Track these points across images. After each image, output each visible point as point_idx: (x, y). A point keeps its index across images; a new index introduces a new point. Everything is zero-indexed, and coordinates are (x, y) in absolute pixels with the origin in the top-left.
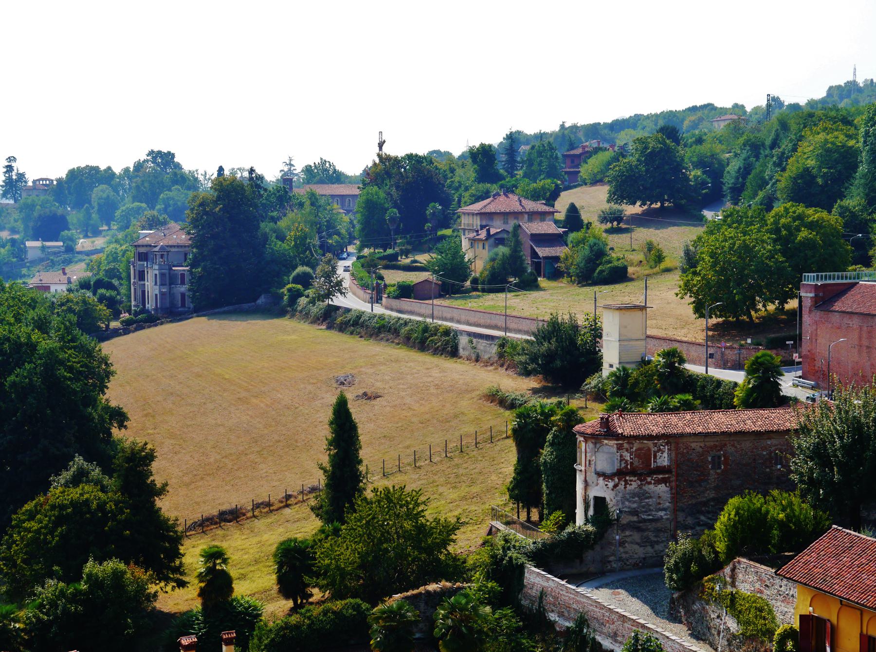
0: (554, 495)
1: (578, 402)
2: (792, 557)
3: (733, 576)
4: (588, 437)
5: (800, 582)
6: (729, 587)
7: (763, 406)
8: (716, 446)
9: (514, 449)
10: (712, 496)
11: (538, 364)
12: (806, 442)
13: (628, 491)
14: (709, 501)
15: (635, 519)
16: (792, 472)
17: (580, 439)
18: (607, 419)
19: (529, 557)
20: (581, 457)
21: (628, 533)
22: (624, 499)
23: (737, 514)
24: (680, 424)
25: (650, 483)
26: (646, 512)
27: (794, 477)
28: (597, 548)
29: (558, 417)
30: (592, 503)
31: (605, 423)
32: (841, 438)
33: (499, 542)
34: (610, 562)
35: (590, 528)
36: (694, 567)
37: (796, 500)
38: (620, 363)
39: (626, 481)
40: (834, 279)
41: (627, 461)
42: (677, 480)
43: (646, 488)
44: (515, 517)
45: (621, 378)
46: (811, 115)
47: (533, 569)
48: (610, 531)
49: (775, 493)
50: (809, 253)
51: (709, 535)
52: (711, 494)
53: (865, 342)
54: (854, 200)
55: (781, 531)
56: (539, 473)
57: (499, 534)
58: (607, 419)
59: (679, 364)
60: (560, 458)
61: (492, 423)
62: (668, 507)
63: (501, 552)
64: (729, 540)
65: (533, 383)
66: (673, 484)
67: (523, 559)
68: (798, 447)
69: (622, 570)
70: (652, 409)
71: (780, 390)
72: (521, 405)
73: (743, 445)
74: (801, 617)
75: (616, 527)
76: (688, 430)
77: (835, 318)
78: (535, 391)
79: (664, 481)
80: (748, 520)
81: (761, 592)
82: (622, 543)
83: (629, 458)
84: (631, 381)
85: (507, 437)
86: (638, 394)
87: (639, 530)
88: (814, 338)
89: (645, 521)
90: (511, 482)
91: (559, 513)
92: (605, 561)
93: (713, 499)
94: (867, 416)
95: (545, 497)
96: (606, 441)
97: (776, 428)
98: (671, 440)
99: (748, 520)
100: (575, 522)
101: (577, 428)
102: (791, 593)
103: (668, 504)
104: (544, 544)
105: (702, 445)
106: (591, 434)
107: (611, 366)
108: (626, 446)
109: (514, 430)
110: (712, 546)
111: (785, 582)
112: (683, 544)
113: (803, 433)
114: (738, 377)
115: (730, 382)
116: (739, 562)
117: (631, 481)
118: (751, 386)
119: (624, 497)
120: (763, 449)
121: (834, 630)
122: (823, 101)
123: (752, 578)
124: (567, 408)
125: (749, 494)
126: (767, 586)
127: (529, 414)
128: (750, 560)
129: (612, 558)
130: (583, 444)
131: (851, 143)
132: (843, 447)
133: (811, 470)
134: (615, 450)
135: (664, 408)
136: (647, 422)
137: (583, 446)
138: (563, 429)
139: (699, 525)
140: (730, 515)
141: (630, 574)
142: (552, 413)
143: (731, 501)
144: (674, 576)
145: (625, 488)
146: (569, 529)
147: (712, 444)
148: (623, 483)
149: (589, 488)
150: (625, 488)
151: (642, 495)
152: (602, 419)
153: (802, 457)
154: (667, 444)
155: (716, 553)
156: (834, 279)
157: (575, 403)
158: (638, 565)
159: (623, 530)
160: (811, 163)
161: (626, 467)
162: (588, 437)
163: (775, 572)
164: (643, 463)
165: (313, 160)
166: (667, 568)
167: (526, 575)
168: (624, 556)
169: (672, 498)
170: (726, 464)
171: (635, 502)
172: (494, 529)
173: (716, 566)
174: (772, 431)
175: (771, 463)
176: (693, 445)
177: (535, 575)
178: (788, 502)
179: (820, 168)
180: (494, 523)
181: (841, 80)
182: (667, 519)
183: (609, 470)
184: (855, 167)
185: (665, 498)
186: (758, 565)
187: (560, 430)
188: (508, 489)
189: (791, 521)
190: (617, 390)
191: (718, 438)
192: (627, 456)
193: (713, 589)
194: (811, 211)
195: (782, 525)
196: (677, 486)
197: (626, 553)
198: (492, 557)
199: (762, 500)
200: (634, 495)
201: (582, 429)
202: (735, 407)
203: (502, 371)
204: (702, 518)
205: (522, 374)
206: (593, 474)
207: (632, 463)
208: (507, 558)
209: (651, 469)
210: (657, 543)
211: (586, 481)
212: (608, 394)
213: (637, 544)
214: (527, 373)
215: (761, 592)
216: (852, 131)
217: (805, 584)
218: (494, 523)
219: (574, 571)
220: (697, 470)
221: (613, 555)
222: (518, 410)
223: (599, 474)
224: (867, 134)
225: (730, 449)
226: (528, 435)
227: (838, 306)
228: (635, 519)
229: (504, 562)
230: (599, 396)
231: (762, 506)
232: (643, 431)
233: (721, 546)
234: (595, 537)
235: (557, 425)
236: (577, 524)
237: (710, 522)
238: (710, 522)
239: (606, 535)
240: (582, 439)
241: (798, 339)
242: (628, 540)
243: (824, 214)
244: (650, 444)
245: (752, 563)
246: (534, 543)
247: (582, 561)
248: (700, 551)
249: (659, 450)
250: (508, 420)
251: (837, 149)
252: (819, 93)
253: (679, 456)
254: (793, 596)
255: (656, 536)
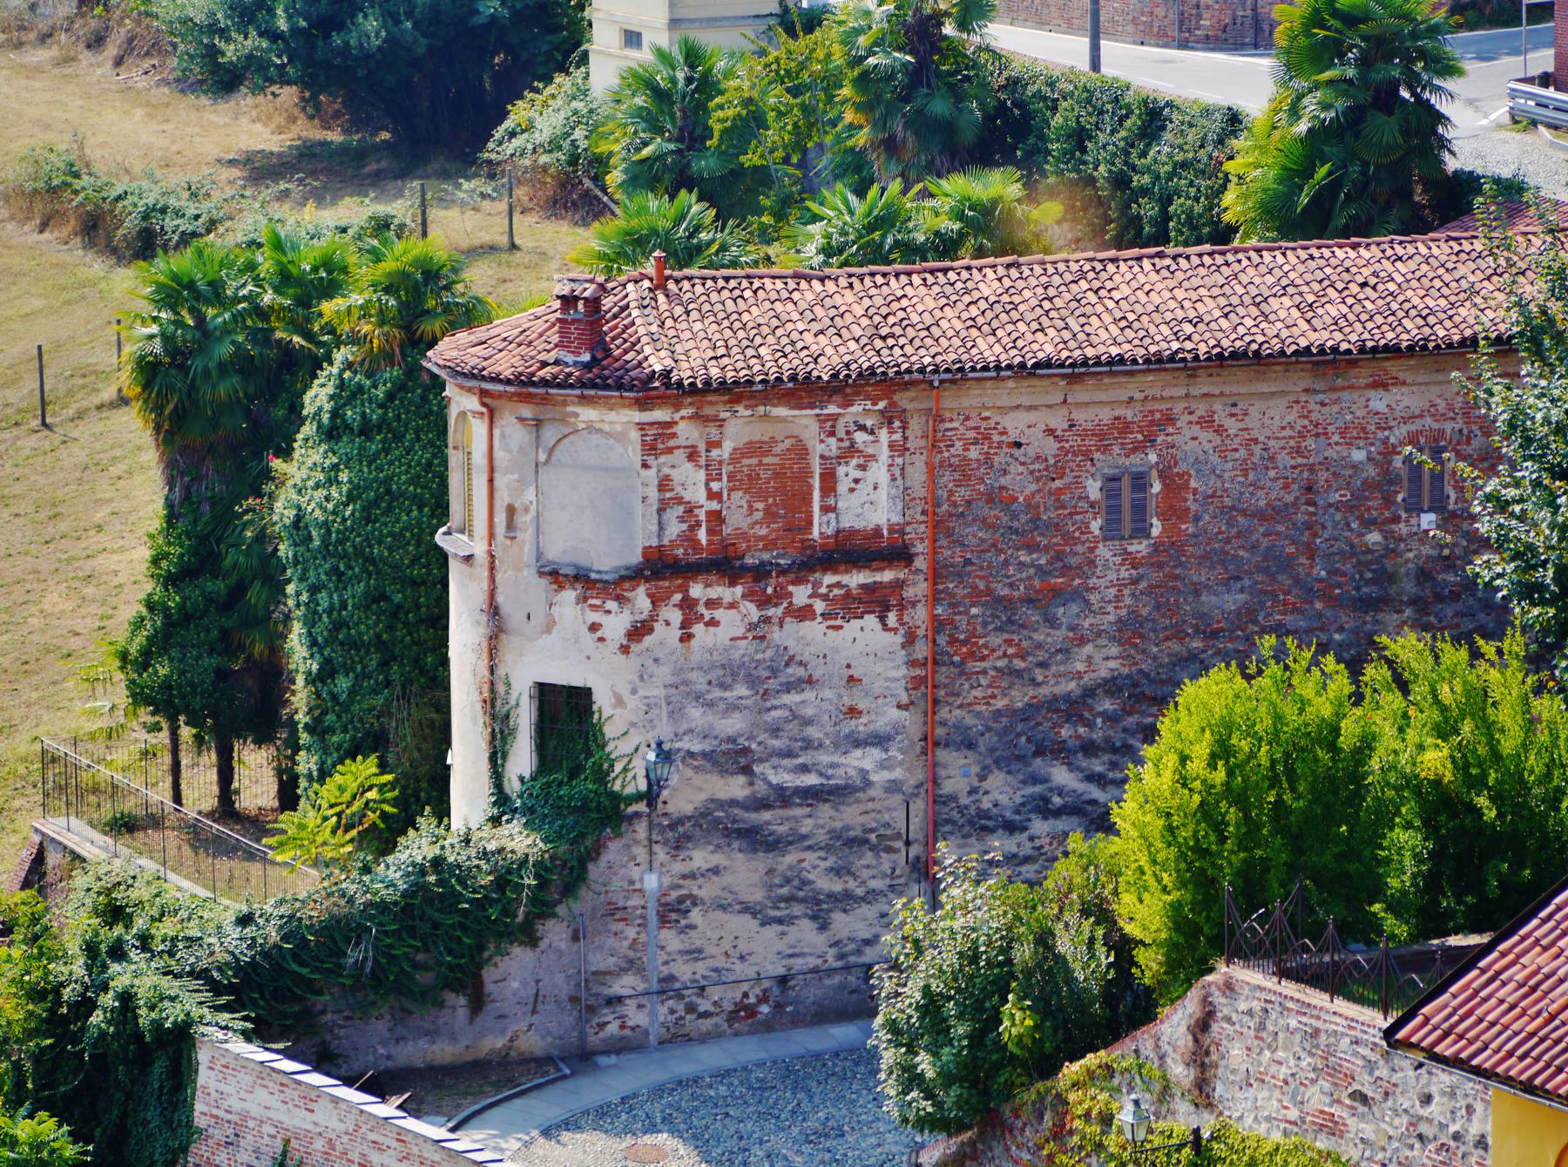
0: (343, 683)
1: (470, 220)
2: (1467, 960)
3: (1202, 1058)
4: (498, 392)
5: (1507, 1080)
6: (1183, 1107)
7: (1359, 230)
8: (1123, 426)
9: (149, 459)
10: (1104, 670)
11: (274, 36)
13: (696, 657)
14: (1089, 693)
15: (736, 787)
16: (1484, 544)
17: (461, 402)
18: (594, 304)
19: (216, 988)
20: (467, 488)
21: (701, 858)
22: (682, 693)
23: (1222, 752)
24: (951, 321)
25: (805, 613)
26: (790, 754)
27: (1492, 569)
28: (554, 933)
29: (357, 299)
30: (525, 720)
31: (585, 318)
33: (74, 920)
34: (615, 1001)
35: (519, 839)
36: (1016, 1021)
37: (1506, 683)
38: (674, 23)
39: (688, 604)
41: (690, 510)
42: (935, 598)
43: (791, 635)
44: (161, 795)
45: (680, 102)
47: (240, 1047)
48: (613, 851)
49: (1407, 647)
51: (1089, 863)
52: (1103, 660)
55: (1430, 827)
56: (271, 575)
57: (80, 881)
58: (594, 304)
59: (963, 25)
60: (374, 501)
61: (45, 332)
62: (898, 728)
63: (78, 968)
64: (1182, 884)
65: (263, 123)
66: (920, 615)
67: (188, 1002)
68: (1512, 425)
69: (675, 1038)
70: (828, 251)
71: (1443, 144)
72: (187, 238)
73: (1253, 421)
75: (641, 829)
76: (988, 350)
78: (261, 170)
79: (877, 601)
80: (1274, 781)
81: (1332, 1127)
82: (673, 911)
83: (700, 496)
84: (722, 114)
85: (123, 401)
86: (762, 177)
87: (755, 840)
89: (784, 797)
90: (138, 623)
91: (365, 768)
92: (589, 999)
93: (1111, 686)
95: (300, 700)
96: (587, 414)
97: (1411, 330)
98: (904, 399)
99: (1274, 781)
100: (443, 812)
101: (450, 350)
102: (1475, 1129)
103: (895, 714)
104: (293, 928)
105: (1058, 421)
106: (518, 380)
107: (632, 38)
108: (687, 432)
109: (148, 370)
110: (1098, 910)
111: (1444, 1078)
112: (971, 907)
113: (1538, 353)
114: (1246, 83)
115: (1207, 112)
116: (1229, 987)
117: (711, 604)
118: (1302, 127)
119: (679, 684)
120: (1355, 433)
123: (1289, 1060)
124: (402, 254)
125: (1280, 654)
126: (1363, 1098)
127: (216, 286)
128: (1284, 973)
129: (624, 985)
130: (479, 428)
134: (634, 454)
135: (879, 248)
136: (798, 307)
137: (473, 436)
138: (389, 358)
139: (1044, 809)
140: (1184, 759)
141: (711, 1057)
142: (330, 280)
143: (1192, 692)
144: (925, 1063)
145: (686, 638)
146: (417, 847)
147: (1106, 415)
148: (676, 616)
149: (508, 644)
150: (686, 638)
151: (773, 676)
152: (568, 301)
153: (1528, 471)
154: (887, 418)
155: (1123, 947)
157: (454, 220)
158: (751, 1012)
159: (678, 846)
161: (689, 538)
162: (498, 392)
163: (1389, 1033)
164: (770, 514)
166: (892, 1026)
167: (205, 1077)
168: (684, 971)
169: (916, 683)
170: (1173, 511)
171: (733, 707)
172: (53, 859)
173: (1126, 1007)
174: (1393, 351)
175: (1389, 502)
176: (1015, 424)
177: (246, 1079)
178: (1469, 692)
180: (54, 826)
182: (893, 787)
183: (608, 558)
185: (878, 686)
186: (1318, 998)
187: (371, 365)
188: (124, 656)
189: (1479, 783)
190: (659, 157)
191: (1131, 388)
192: (692, 483)
193: (1107, 1120)
195: (1441, 806)
196: (937, 625)
197: (695, 954)
198: (36, 994)
199: (1341, 684)
200: (730, 673)
201: (471, 361)
202: (1222, 235)
203: (97, 67)
204: (1061, 776)
205: (197, 87)
206: (530, 574)
207: (716, 518)
208: (108, 1000)
209: (807, 545)
210: (845, 900)
211: (494, 610)
212: (615, 178)
213: (747, 909)
214: (225, 81)
215: (1332, 1127)
217: (1529, 1088)
218: (54, 826)
219: (442, 1051)
220: (1032, 547)
221: (632, 965)
222: (165, 266)
223: (555, 576)
225: (1190, 441)
226: (219, 396)
228: (736, 787)
229: (97, 1018)
230: (575, 190)
231: (1339, 716)
232: (767, 362)
233: (1142, 912)
234: (543, 883)
235: (355, 339)
236: (457, 821)
237: (1095, 793)
238: (1095, 793)
239: (595, 871)
240: (472, 403)
242: (706, 890)
244: (803, 422)
245: (1289, 988)
246: (244, 920)
247: (478, 1002)
248: (1044, 939)
249: (851, 451)
250: (120, 311)
253: (947, 478)
254: (1481, 1143)
255: (837, 871)
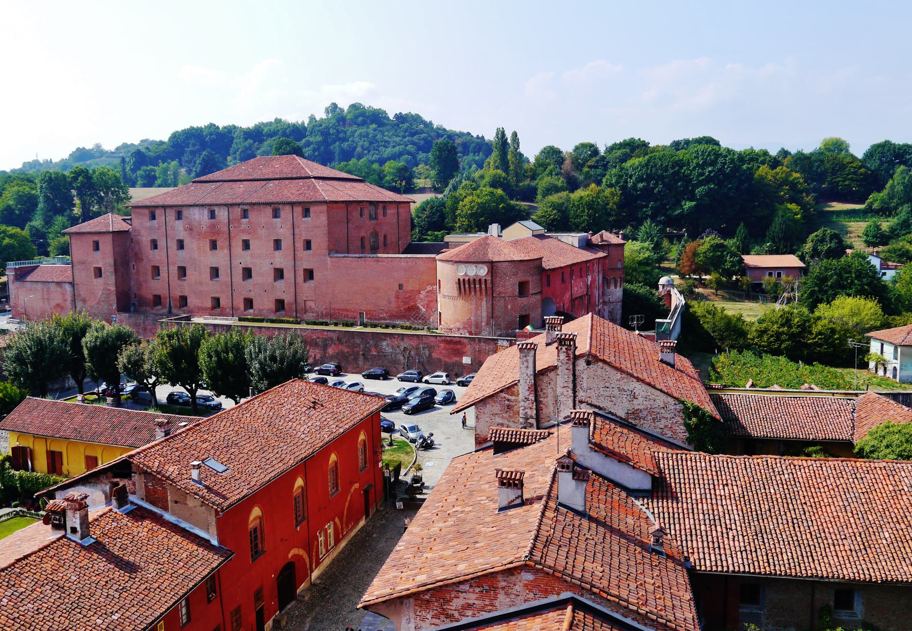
12: (11, 354)
27: (6, 373)
32: (30, 349)
37: (9, 385)
40: (27, 264)
46: (10, 177)
50: (11, 251)
53: (46, 297)
54: (37, 222)
74: (13, 448)
77: (28, 285)
88: (17, 297)
94: (44, 336)
121: (32, 451)
122: (20, 170)
131: (33, 192)
132: (32, 353)
133: (15, 368)
156: (27, 264)
160: (11, 202)
165: (573, 148)
179: (16, 205)
181: (30, 159)
184: (36, 205)
194: (10, 228)
216: (33, 186)
224: (41, 187)
227: (29, 278)
241: (7, 298)
243: (18, 230)
251: (26, 195)
252: (18, 166)
